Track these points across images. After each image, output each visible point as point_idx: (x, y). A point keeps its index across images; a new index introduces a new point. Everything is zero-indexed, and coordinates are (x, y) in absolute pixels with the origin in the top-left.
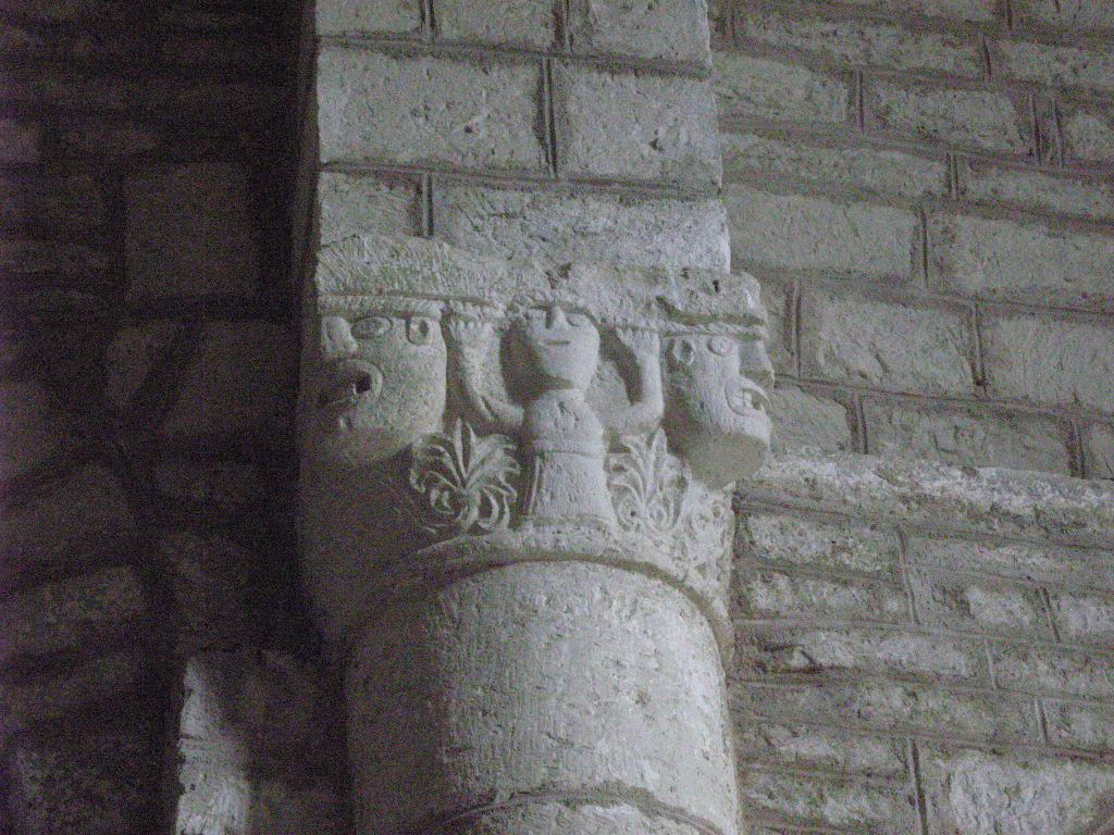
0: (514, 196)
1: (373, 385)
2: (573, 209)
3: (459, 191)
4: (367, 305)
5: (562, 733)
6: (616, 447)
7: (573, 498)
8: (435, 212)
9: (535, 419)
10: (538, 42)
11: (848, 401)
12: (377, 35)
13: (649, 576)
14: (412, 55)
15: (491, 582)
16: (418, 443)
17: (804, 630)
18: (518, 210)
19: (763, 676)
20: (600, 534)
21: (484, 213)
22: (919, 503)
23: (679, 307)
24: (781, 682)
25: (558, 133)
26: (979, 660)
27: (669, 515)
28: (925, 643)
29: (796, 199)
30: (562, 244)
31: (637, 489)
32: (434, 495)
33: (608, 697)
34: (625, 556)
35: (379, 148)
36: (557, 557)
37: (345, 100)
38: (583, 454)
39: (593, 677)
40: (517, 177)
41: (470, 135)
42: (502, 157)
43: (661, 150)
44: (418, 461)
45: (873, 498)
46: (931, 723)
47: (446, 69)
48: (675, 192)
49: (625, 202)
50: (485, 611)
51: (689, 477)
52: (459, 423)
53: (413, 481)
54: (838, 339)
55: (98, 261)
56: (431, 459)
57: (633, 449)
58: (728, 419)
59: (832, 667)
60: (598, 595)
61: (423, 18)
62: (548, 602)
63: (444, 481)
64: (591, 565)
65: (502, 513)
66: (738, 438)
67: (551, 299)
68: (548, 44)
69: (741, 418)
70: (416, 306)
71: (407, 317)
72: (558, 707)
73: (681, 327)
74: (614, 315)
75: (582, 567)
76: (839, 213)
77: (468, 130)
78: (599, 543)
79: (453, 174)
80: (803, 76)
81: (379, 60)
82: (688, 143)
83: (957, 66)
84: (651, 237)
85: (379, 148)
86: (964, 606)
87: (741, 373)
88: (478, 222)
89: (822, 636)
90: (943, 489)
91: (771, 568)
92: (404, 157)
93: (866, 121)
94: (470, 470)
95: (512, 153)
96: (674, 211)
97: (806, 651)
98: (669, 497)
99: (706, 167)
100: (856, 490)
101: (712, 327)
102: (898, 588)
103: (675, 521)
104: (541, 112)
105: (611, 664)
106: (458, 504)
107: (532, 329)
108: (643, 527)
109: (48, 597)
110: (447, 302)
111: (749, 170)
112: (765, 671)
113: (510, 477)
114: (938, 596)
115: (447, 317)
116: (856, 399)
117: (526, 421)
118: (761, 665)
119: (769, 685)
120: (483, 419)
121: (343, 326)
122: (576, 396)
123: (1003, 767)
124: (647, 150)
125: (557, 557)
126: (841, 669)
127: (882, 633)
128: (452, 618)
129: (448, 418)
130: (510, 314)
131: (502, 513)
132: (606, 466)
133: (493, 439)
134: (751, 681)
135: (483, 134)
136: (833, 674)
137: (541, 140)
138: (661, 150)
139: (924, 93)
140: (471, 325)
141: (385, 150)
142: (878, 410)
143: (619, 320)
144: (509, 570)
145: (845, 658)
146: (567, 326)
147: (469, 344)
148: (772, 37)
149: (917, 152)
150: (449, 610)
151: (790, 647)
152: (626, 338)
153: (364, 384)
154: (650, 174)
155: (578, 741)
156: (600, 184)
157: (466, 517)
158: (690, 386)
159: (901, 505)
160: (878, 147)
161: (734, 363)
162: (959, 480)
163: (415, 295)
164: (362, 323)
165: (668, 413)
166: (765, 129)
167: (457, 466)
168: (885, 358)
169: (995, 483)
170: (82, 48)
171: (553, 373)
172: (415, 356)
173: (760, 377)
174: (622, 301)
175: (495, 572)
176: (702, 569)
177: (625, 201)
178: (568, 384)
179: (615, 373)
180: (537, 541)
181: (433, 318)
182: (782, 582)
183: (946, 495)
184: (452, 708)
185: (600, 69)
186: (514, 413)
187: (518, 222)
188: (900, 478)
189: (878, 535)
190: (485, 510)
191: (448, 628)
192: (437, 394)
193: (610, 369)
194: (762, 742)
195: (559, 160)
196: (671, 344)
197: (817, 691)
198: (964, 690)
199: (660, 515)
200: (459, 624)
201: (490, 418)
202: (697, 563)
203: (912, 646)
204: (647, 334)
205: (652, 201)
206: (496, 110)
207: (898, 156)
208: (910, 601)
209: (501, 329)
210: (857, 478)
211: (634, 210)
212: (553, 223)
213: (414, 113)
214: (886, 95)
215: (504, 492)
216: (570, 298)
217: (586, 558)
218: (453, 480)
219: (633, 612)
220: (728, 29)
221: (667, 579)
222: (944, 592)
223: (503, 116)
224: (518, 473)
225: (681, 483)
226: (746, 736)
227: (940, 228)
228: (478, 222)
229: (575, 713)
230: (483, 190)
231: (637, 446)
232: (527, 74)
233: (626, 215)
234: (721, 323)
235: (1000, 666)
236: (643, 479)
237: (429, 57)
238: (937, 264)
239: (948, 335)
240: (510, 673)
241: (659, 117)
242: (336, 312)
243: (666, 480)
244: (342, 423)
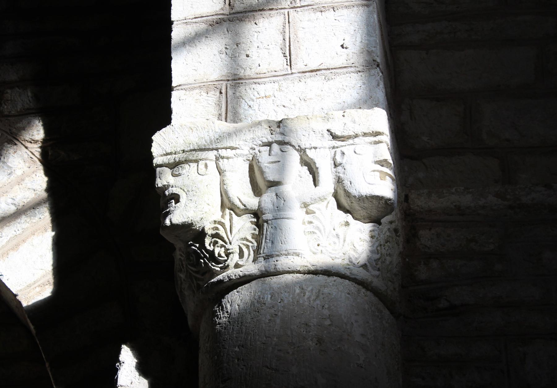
18: (271, 94)
21: (254, 98)
30: (293, 107)
31: (320, 231)
38: (288, 218)
53: (207, 245)
56: (214, 232)
62: (271, 298)
65: (249, 255)
107: (262, 157)
150: (227, 309)
158: (378, 163)
167: (226, 233)
187: (270, 100)
201: (242, 207)
218: (226, 243)
224: (257, 233)
236: (324, 226)
237: (228, 22)
240: (251, 337)
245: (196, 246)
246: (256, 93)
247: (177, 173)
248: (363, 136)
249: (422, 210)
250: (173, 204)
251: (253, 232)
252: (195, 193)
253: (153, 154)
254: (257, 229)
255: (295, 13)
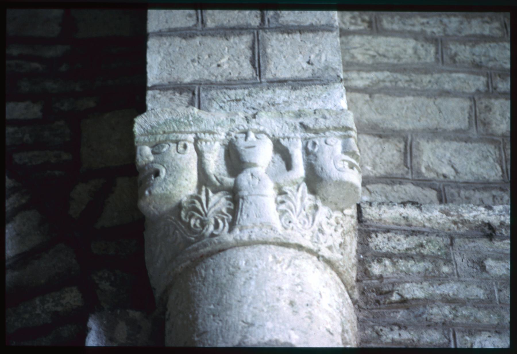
0: (239, 92)
1: (161, 174)
2: (268, 95)
3: (213, 92)
4: (158, 139)
5: (249, 320)
6: (281, 192)
7: (258, 216)
8: (201, 102)
9: (239, 182)
10: (253, 24)
11: (437, 188)
12: (175, 30)
13: (299, 250)
14: (192, 36)
15: (219, 259)
16: (185, 199)
17: (399, 283)
18: (241, 97)
19: (378, 306)
20: (272, 232)
21: (225, 100)
22: (462, 224)
23: (311, 126)
24: (388, 308)
25: (261, 61)
26: (490, 291)
27: (309, 221)
28: (463, 286)
29: (410, 98)
31: (292, 210)
32: (193, 222)
33: (273, 302)
34: (285, 241)
35: (176, 77)
36: (250, 243)
37: (160, 59)
38: (262, 195)
39: (266, 295)
40: (242, 83)
41: (219, 68)
42: (235, 75)
43: (312, 64)
44: (185, 208)
45: (439, 223)
46: (464, 321)
47: (209, 41)
48: (318, 82)
49: (294, 89)
50: (216, 271)
51: (319, 204)
52: (204, 188)
54: (432, 160)
55: (66, 156)
57: (289, 192)
58: (335, 174)
59: (413, 299)
60: (271, 259)
61: (198, 19)
62: (246, 264)
63: (197, 215)
64: (268, 246)
65: (224, 226)
66: (341, 183)
67: (247, 128)
68: (258, 24)
69: (341, 173)
70: (181, 136)
71: (177, 142)
72: (248, 309)
73: (312, 135)
74: (278, 133)
75: (263, 247)
76: (431, 103)
77: (219, 66)
78: (271, 236)
79: (210, 85)
80: (412, 43)
81: (177, 40)
82: (326, 60)
83: (490, 31)
84: (306, 102)
85: (176, 77)
86: (483, 268)
87: (342, 153)
88: (222, 104)
89: (408, 285)
90: (475, 216)
91: (379, 257)
92: (188, 80)
93: (445, 60)
94: (209, 209)
95: (240, 73)
96: (318, 89)
97: (400, 293)
98: (309, 214)
99: (334, 70)
100: (429, 220)
101: (327, 133)
102: (448, 261)
103: (312, 225)
104: (254, 54)
105: (276, 289)
106: (203, 224)
107: (238, 143)
108: (295, 228)
109: (38, 302)
110: (196, 134)
111: (386, 88)
112: (380, 304)
113: (229, 210)
114: (470, 264)
115: (197, 140)
116: (441, 187)
117: (236, 182)
118: (378, 302)
119: (382, 310)
120: (215, 185)
121: (147, 150)
122: (261, 170)
123: (500, 338)
124: (305, 65)
125: (250, 243)
126: (417, 299)
127: (439, 282)
128: (201, 277)
129: (199, 187)
130: (228, 137)
131: (224, 226)
132: (276, 201)
133: (220, 194)
134: (373, 309)
135: (226, 66)
136: (414, 303)
137: (253, 66)
138: (312, 64)
139: (473, 46)
140: (208, 143)
141: (178, 78)
142: (453, 191)
143: (281, 135)
144: (228, 252)
145: (419, 294)
146: (255, 139)
147: (208, 152)
148: (396, 27)
149: (472, 73)
151: (390, 292)
152: (284, 143)
153: (157, 173)
154: (307, 75)
155: (257, 324)
156: (282, 82)
157: (207, 230)
158: (316, 160)
159: (453, 226)
160: (451, 72)
161: (339, 148)
162: (483, 212)
163: (181, 132)
164: (156, 149)
165: (307, 175)
166: (394, 68)
168: (457, 167)
169: (501, 212)
170: (63, 68)
171: (247, 160)
172: (181, 159)
173: (353, 154)
174: (282, 126)
175: (221, 253)
176: (330, 248)
177: (294, 88)
178: (255, 165)
179: (280, 159)
180: (240, 237)
181: (190, 142)
182: (387, 262)
183: (476, 219)
184: (199, 316)
185: (283, 32)
186: (229, 181)
187: (241, 103)
188: (452, 213)
189: (440, 239)
190: (217, 226)
191: (200, 281)
192: (193, 176)
193: (278, 158)
194: (375, 335)
195: (262, 74)
196: (307, 144)
197: (406, 311)
198: (482, 305)
199: (305, 223)
200: (205, 279)
201: (218, 184)
202: (326, 245)
203: (455, 287)
204: (295, 140)
205: (307, 87)
206: (232, 55)
207: (461, 75)
208: (455, 267)
209: (224, 145)
210: (430, 214)
211: (298, 92)
212: (259, 101)
213: (193, 61)
214: (453, 48)
215: (225, 217)
216: (256, 127)
217: (265, 243)
219: (289, 266)
220: (374, 25)
221: (310, 251)
222: (473, 262)
223: (236, 58)
225: (316, 208)
226: (366, 332)
227: (483, 105)
228: (222, 104)
229: (257, 311)
230: (225, 90)
231: (291, 191)
232: (247, 39)
233: (294, 94)
234: (331, 131)
235: (502, 293)
237: (201, 36)
238: (482, 122)
239: (489, 154)
241: (311, 51)
242: (145, 143)
243: (307, 207)
244: (147, 193)
245: (171, 219)
246: (227, 97)
247: (157, 151)
248: (333, 130)
249: (373, 218)
250: (153, 178)
251: (228, 206)
252: (174, 169)
253: (135, 133)
254: (232, 204)
255: (264, 34)
